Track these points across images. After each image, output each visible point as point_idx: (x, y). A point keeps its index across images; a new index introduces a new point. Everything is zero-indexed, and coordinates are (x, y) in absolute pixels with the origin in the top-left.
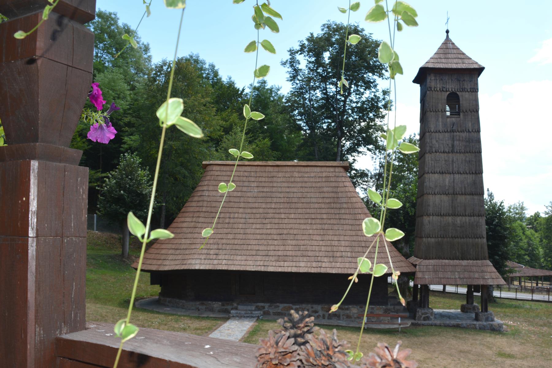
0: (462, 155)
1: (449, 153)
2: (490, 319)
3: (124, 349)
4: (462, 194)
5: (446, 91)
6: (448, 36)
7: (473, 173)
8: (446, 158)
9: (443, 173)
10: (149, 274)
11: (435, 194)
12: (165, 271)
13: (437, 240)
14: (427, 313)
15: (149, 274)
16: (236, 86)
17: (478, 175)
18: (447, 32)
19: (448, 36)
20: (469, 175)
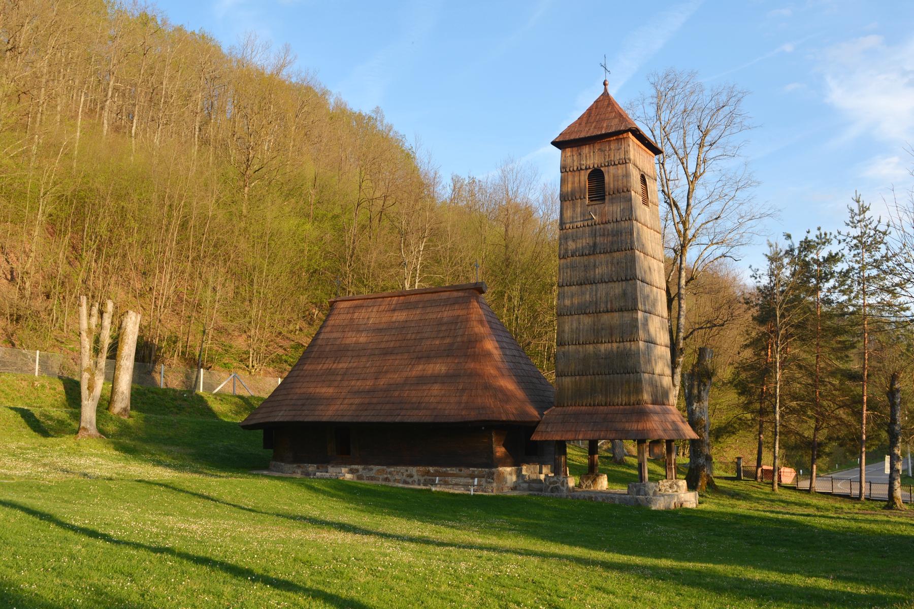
0: (607, 255)
1: (589, 254)
2: (642, 493)
3: (262, 445)
4: (607, 311)
5: (586, 169)
6: (606, 89)
7: (622, 280)
8: (586, 263)
9: (581, 284)
10: (260, 432)
11: (571, 314)
12: (275, 423)
13: (574, 378)
14: (556, 483)
15: (260, 432)
16: (189, 29)
17: (630, 282)
18: (605, 84)
19: (606, 89)
20: (616, 284)
